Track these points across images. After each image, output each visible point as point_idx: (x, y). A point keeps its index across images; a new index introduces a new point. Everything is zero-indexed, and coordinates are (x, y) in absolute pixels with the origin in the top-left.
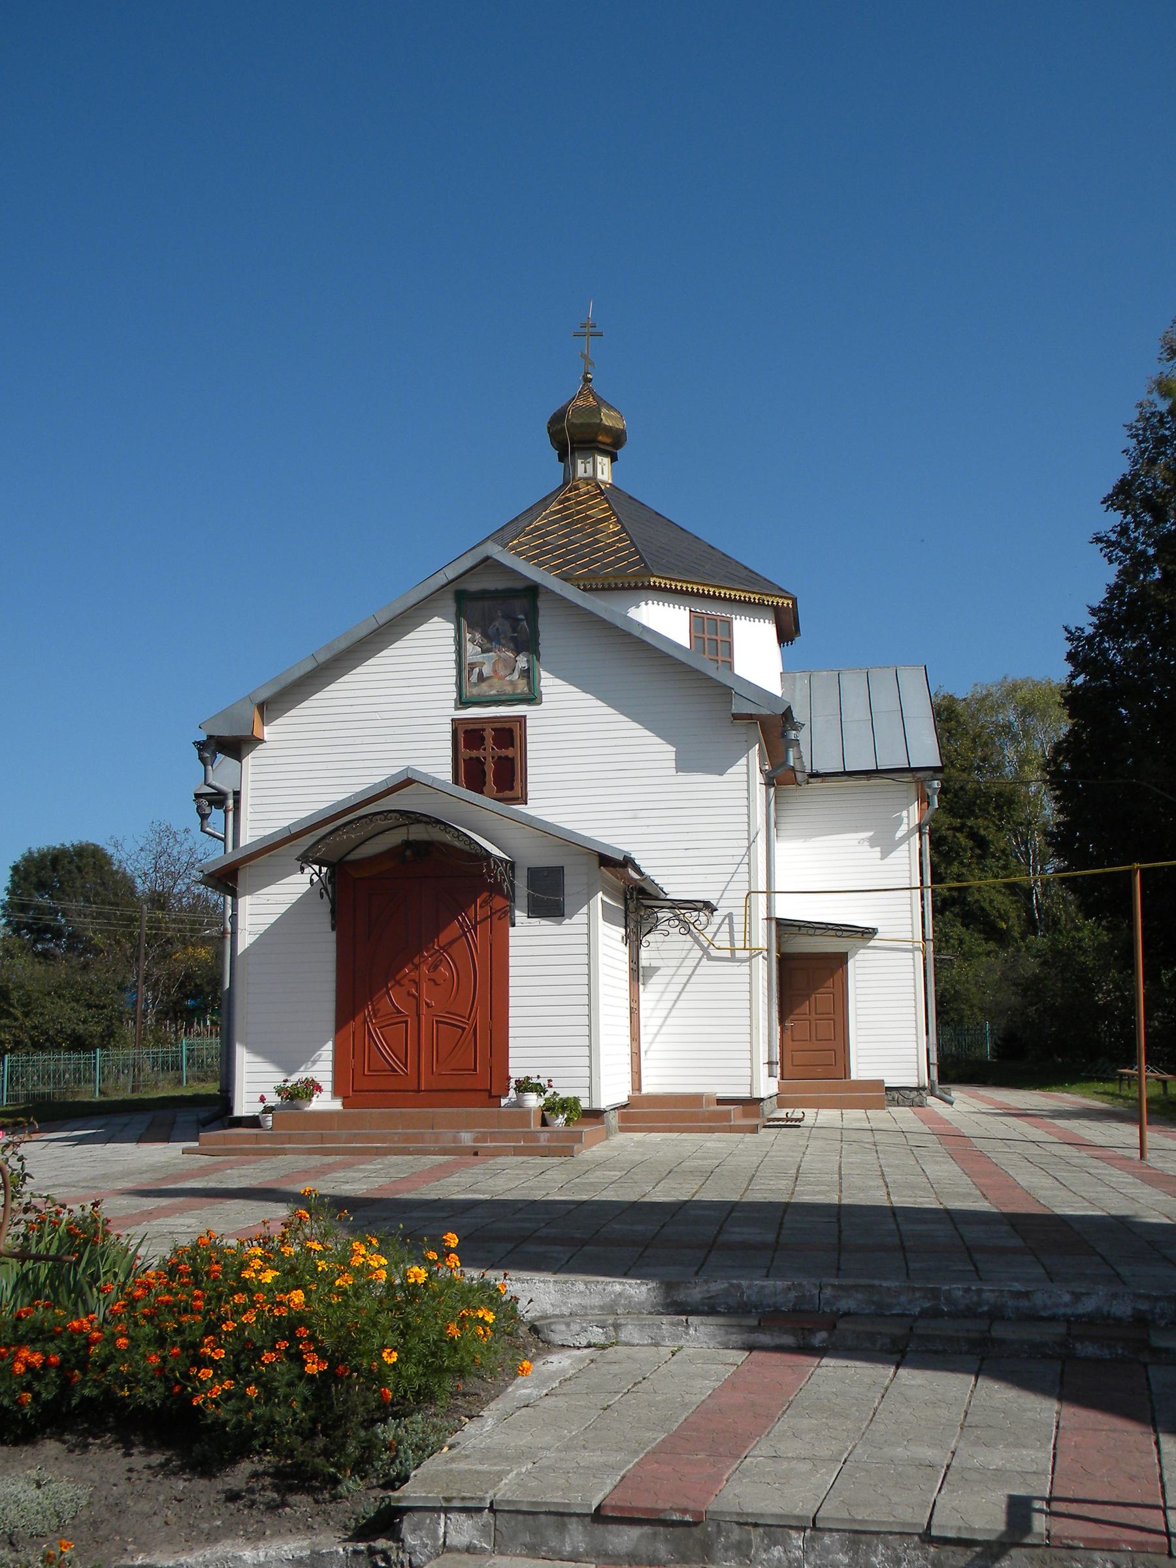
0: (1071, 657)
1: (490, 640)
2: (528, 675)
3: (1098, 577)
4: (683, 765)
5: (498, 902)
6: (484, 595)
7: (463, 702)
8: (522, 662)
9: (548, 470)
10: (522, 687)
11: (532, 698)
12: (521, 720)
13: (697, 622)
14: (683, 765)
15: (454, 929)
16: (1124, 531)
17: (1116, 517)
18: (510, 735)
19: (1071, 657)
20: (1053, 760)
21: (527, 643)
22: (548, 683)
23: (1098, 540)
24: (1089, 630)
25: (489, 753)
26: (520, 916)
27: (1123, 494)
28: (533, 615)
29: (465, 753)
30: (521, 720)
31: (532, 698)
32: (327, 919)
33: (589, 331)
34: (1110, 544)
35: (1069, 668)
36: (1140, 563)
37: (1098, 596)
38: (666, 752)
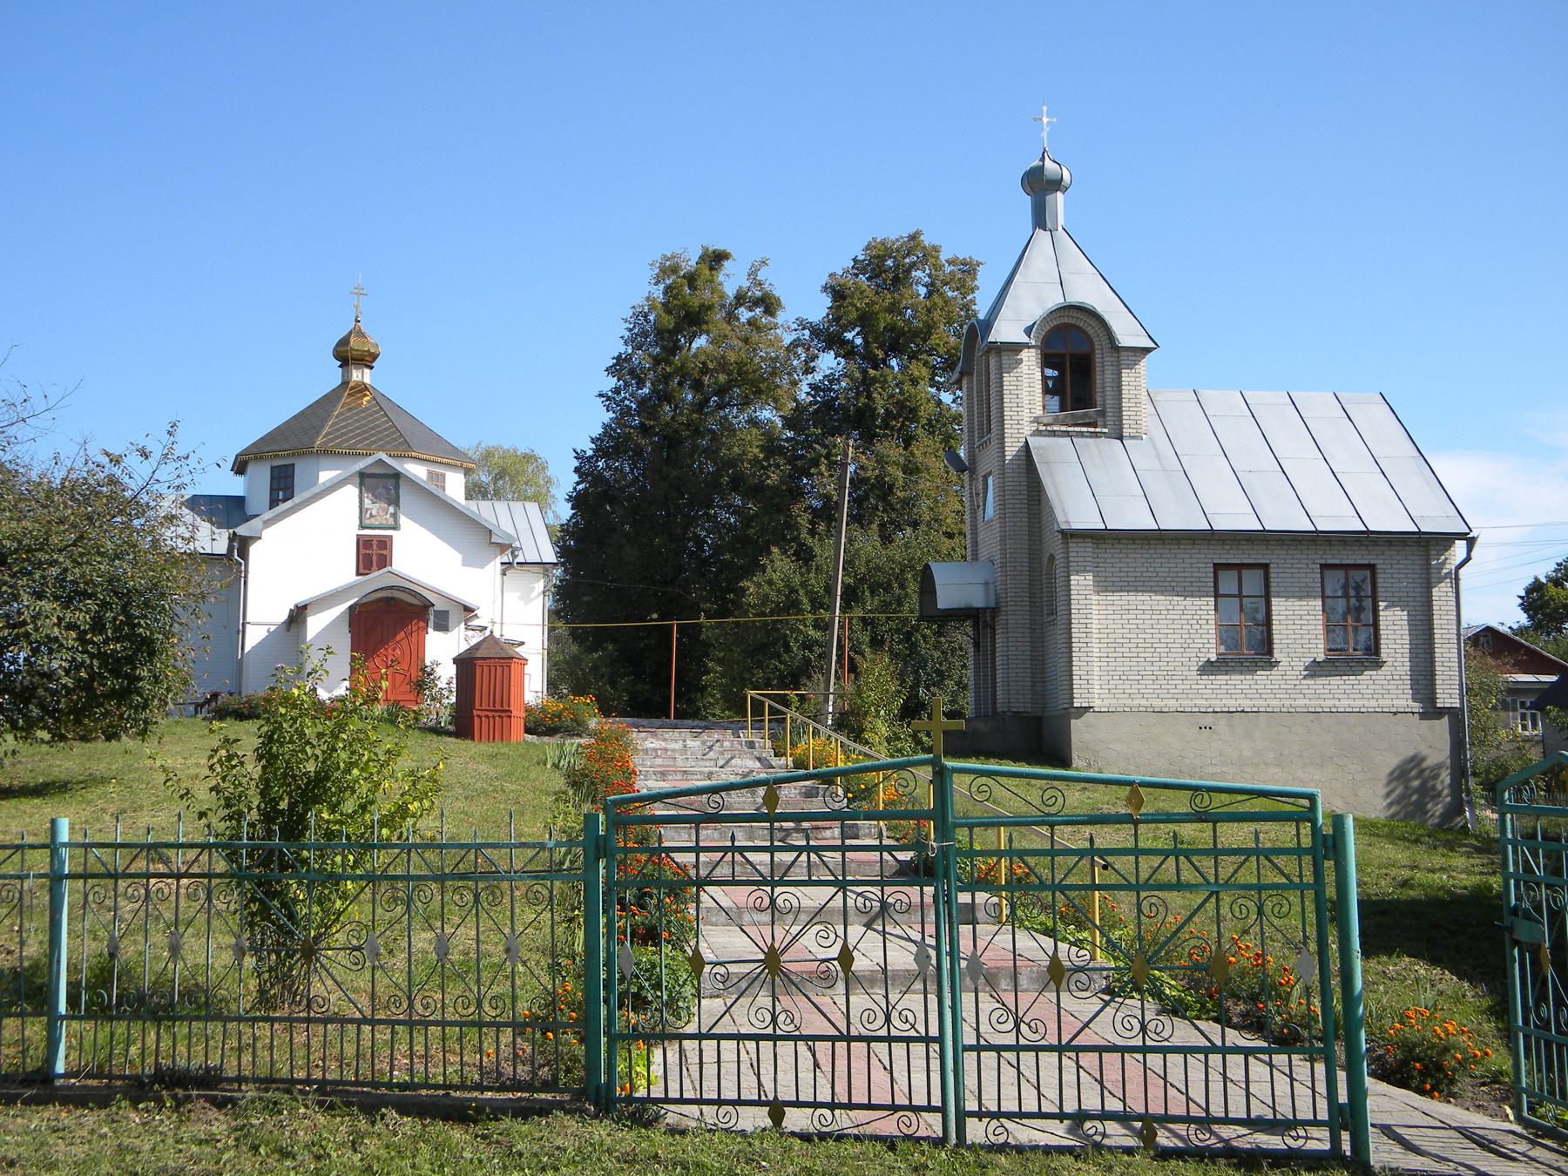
0: (577, 470)
1: (377, 498)
2: (395, 516)
3: (597, 418)
4: (465, 564)
5: (422, 624)
6: (373, 476)
7: (362, 527)
8: (391, 510)
9: (331, 375)
10: (391, 521)
11: (396, 527)
12: (390, 537)
13: (430, 473)
14: (465, 564)
15: (402, 634)
16: (617, 391)
17: (612, 382)
18: (385, 543)
19: (577, 470)
20: (563, 538)
21: (395, 502)
22: (403, 520)
23: (601, 395)
24: (589, 453)
25: (375, 551)
26: (430, 630)
27: (620, 367)
28: (397, 488)
29: (362, 551)
30: (390, 537)
31: (396, 527)
32: (1494, 624)
33: (359, 292)
34: (609, 399)
35: (576, 478)
36: (626, 412)
37: (597, 431)
38: (458, 557)
